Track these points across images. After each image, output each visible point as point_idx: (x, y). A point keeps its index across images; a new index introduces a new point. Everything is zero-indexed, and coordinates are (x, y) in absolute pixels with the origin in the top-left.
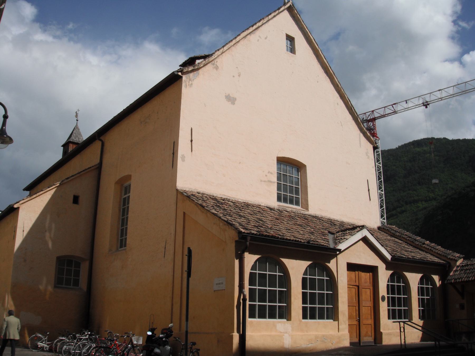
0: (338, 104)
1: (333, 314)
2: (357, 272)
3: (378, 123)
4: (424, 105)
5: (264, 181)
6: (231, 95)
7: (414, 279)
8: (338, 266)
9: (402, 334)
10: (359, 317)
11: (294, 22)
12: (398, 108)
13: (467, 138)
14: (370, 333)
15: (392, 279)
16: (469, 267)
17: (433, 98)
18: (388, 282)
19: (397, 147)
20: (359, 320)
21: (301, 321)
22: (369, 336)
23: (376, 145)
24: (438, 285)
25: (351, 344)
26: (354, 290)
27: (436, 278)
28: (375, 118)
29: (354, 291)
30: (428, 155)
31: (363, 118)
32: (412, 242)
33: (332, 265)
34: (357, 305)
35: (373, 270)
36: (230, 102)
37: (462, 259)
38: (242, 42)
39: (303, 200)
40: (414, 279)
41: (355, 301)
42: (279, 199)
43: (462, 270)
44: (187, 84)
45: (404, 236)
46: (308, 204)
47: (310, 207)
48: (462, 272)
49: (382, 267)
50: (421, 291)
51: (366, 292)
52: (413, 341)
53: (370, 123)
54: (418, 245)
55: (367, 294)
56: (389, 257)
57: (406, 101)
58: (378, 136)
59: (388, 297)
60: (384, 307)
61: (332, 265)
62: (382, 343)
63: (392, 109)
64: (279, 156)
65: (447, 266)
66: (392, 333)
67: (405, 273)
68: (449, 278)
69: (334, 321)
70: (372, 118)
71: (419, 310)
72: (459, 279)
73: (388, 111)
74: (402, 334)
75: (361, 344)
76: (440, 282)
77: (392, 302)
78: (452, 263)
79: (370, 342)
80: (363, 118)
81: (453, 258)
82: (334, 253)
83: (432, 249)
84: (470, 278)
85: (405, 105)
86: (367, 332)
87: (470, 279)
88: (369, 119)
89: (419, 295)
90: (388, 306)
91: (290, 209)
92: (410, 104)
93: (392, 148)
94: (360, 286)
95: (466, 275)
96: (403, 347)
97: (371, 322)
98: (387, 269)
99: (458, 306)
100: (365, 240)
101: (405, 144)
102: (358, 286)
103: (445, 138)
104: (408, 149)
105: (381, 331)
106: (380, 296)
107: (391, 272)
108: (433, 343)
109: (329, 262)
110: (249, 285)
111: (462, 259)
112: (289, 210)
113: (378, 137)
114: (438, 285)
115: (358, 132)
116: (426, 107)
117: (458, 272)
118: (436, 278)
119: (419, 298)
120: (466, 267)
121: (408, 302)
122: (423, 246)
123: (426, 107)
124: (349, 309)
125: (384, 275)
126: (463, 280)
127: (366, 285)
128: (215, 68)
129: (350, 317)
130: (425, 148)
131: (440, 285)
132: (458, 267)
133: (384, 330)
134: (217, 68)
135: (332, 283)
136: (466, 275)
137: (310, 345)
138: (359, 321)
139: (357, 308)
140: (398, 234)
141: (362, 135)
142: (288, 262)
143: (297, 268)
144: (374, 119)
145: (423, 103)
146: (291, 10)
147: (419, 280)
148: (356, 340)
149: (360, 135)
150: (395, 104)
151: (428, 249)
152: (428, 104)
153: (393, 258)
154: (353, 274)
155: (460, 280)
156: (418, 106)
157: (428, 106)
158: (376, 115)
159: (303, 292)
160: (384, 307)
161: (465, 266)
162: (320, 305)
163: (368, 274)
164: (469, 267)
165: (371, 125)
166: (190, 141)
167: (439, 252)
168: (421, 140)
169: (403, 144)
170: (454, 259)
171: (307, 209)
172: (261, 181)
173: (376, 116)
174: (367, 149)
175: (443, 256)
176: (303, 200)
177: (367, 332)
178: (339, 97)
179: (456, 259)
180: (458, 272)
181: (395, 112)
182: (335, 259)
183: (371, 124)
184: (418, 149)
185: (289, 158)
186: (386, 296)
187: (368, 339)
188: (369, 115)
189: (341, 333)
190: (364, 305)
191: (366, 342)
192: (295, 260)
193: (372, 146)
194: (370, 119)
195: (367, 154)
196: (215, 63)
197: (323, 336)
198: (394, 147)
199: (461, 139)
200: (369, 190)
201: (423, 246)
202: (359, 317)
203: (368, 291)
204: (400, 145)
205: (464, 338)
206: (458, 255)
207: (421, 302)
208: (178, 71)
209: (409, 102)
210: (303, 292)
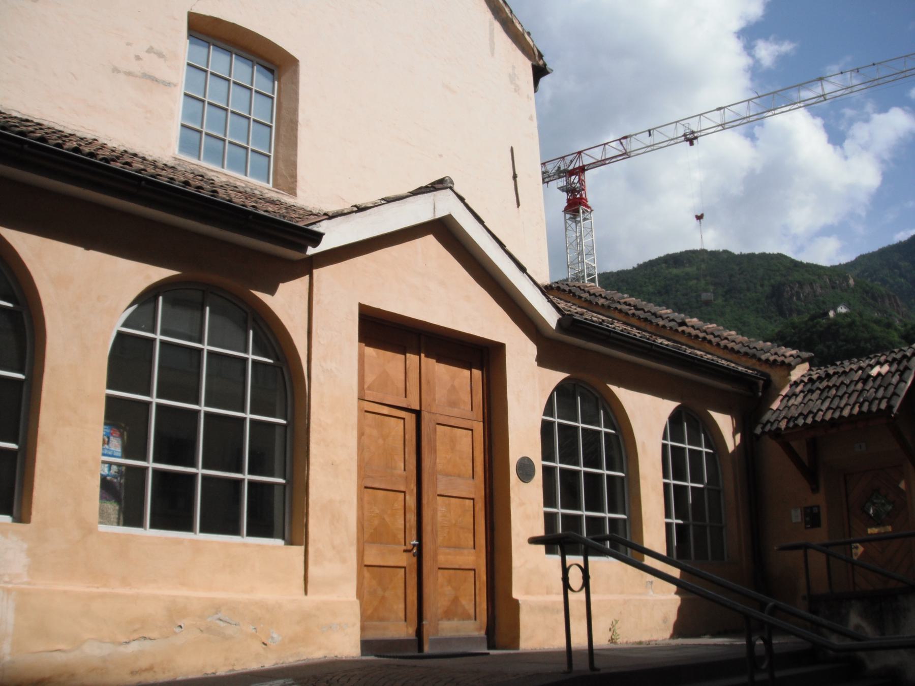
1: (274, 513)
2: (412, 358)
3: (589, 175)
4: (687, 140)
5: (129, 74)
7: (648, 415)
8: (319, 314)
9: (577, 599)
10: (420, 537)
12: (632, 145)
13: (767, 252)
14: (467, 604)
15: (563, 396)
16: (834, 380)
17: (706, 124)
18: (548, 410)
19: (636, 266)
20: (420, 547)
21: (89, 531)
22: (465, 617)
24: (731, 447)
25: (367, 646)
26: (396, 427)
27: (724, 422)
28: (584, 166)
29: (397, 429)
30: (694, 282)
31: (559, 168)
32: (646, 320)
33: (285, 301)
34: (413, 486)
35: (483, 356)
37: (806, 366)
39: (281, 165)
40: (648, 415)
41: (401, 469)
42: (185, 146)
43: (811, 391)
45: (619, 307)
46: (294, 177)
48: (815, 395)
49: (520, 352)
50: (674, 463)
51: (453, 441)
52: (645, 638)
53: (573, 177)
54: (664, 327)
55: (455, 453)
56: (550, 316)
57: (649, 131)
58: (589, 204)
59: (548, 472)
60: (527, 507)
61: (285, 301)
62: (517, 646)
63: (621, 148)
64: (195, 10)
65: (761, 383)
66: (558, 602)
67: (614, 388)
68: (768, 416)
69: (290, 542)
70: (577, 166)
71: (668, 526)
72: (805, 417)
73: (611, 153)
74: (577, 599)
75: (427, 649)
76: (738, 437)
77: (561, 489)
78: (775, 375)
79: (469, 640)
80: (559, 168)
81: (780, 359)
83: (710, 337)
84: (842, 409)
85: (648, 141)
86: (455, 600)
87: (846, 413)
88: (571, 168)
89: (665, 475)
90: (549, 500)
91: (224, 179)
92: (657, 137)
93: (625, 268)
94: (425, 416)
95: (827, 404)
96: (581, 665)
97: (473, 558)
98: (544, 360)
99: (796, 516)
101: (650, 262)
102: (418, 414)
103: (726, 252)
104: (655, 269)
105: (516, 595)
106: (514, 459)
107: (559, 376)
108: (741, 642)
109: (272, 291)
111: (806, 366)
112: (210, 175)
113: (589, 207)
114: (731, 447)
115: (489, 15)
116: (692, 144)
117: (800, 399)
118: (724, 422)
119: (666, 486)
120: (825, 383)
121: (625, 494)
122: (680, 329)
123: (692, 144)
124: (360, 500)
125: (530, 387)
126: (818, 418)
127: (455, 412)
129: (370, 534)
130: (688, 269)
131: (737, 448)
132: (796, 384)
133: (527, 593)
135: (284, 378)
136: (827, 404)
137: (134, 647)
138: (419, 556)
139: (412, 501)
140: (601, 301)
141: (497, 26)
143: (88, 296)
144: (582, 169)
145: (685, 135)
147: (665, 419)
148: (402, 630)
149: (491, 25)
150: (625, 138)
151: (697, 337)
152: (696, 138)
153: (568, 323)
154: (391, 364)
155: (809, 420)
156: (673, 141)
157: (695, 142)
158: (586, 160)
159: (109, 398)
160: (527, 507)
161: (820, 379)
162: (213, 462)
163: (467, 373)
164: (834, 380)
165: (576, 181)
167: (730, 345)
168: (682, 253)
169: (647, 260)
170: (783, 363)
171: (292, 192)
172: (116, 70)
173: (585, 163)
174: (514, 67)
175: (746, 354)
176: (281, 165)
177: (455, 600)
179: (787, 361)
180: (800, 399)
181: (626, 155)
182: (307, 277)
183: (575, 179)
184: (675, 271)
185: (234, 25)
186: (539, 463)
187: (458, 623)
188: (571, 161)
189: (314, 597)
190: (441, 489)
191: (448, 641)
192: (78, 251)
193: (529, 64)
194: (574, 169)
195: (513, 78)
197: (217, 607)
198: (630, 267)
199: (757, 253)
200: (515, 177)
201: (680, 329)
202: (420, 537)
203: (464, 438)
204: (641, 262)
205: (855, 620)
206: (794, 352)
207: (675, 500)
209: (655, 133)
210: (109, 398)
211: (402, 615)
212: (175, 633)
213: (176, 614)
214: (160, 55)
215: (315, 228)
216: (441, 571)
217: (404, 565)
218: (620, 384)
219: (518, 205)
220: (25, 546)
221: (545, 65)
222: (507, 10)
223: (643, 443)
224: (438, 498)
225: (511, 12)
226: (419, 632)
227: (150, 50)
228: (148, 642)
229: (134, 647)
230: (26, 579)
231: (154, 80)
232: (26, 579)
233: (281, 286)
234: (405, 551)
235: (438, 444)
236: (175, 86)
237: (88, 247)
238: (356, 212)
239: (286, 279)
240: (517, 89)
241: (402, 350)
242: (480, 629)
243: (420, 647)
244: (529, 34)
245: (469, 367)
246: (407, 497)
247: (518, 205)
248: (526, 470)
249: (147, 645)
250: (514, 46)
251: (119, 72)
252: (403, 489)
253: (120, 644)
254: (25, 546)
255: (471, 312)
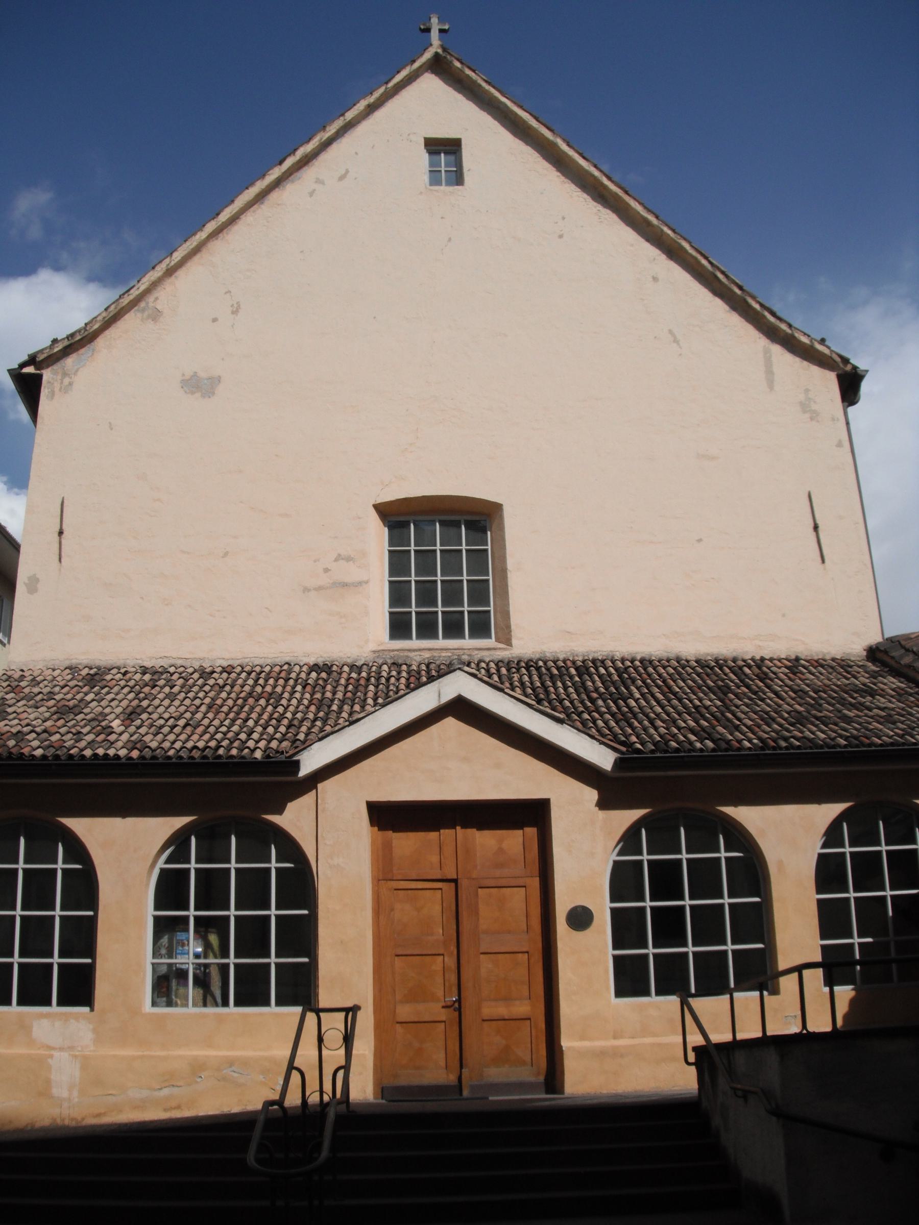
0: (655, 279)
2: (446, 833)
5: (319, 588)
6: (202, 374)
11: (460, 97)
23: (849, 368)
25: (383, 1090)
33: (294, 818)
35: (533, 814)
36: (198, 395)
38: (248, 218)
39: (499, 615)
44: (57, 390)
47: (516, 632)
56: (603, 758)
61: (294, 818)
62: (561, 1091)
75: (466, 1093)
82: (280, 780)
94: (464, 883)
100: (462, 709)
109: (280, 811)
110: (818, 892)
115: (762, 342)
128: (149, 317)
134: (156, 316)
137: (166, 1092)
138: (458, 1007)
141: (777, 350)
142: (750, 817)
146: (439, 66)
166: (56, 535)
171: (508, 642)
172: (306, 590)
174: (807, 391)
176: (499, 615)
178: (663, 257)
182: (314, 791)
196: (151, 304)
208: (23, 365)
211: (443, 1063)
212: (197, 1082)
213: (197, 1068)
214: (349, 559)
215: (295, 758)
216: (486, 1024)
217: (444, 1018)
218: (736, 804)
219: (823, 561)
220: (91, 1027)
221: (855, 368)
222: (784, 327)
223: (780, 863)
224: (482, 956)
225: (790, 326)
226: (460, 1079)
227: (339, 558)
228: (176, 1089)
229: (166, 1092)
230: (92, 1048)
231: (345, 585)
232: (92, 1048)
233: (289, 804)
234: (443, 1007)
235: (481, 907)
236: (367, 582)
237: (124, 816)
238: (348, 726)
239: (291, 800)
240: (814, 416)
241: (436, 828)
242: (538, 1074)
243: (461, 1094)
244: (822, 341)
245: (521, 827)
246: (446, 959)
247: (823, 561)
248: (581, 918)
249: (176, 1091)
250: (805, 363)
251: (309, 590)
252: (441, 952)
253: (155, 1090)
254: (91, 1027)
255: (511, 777)
